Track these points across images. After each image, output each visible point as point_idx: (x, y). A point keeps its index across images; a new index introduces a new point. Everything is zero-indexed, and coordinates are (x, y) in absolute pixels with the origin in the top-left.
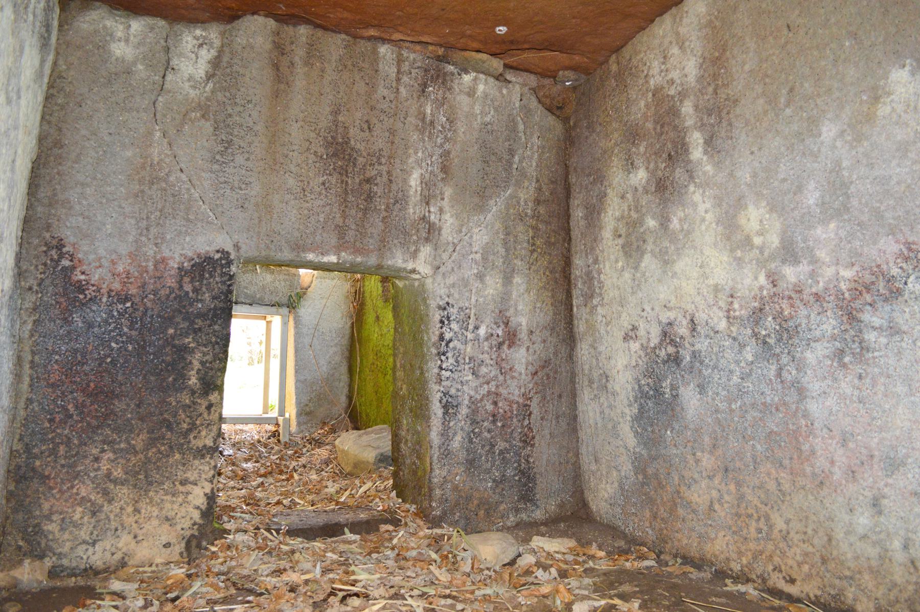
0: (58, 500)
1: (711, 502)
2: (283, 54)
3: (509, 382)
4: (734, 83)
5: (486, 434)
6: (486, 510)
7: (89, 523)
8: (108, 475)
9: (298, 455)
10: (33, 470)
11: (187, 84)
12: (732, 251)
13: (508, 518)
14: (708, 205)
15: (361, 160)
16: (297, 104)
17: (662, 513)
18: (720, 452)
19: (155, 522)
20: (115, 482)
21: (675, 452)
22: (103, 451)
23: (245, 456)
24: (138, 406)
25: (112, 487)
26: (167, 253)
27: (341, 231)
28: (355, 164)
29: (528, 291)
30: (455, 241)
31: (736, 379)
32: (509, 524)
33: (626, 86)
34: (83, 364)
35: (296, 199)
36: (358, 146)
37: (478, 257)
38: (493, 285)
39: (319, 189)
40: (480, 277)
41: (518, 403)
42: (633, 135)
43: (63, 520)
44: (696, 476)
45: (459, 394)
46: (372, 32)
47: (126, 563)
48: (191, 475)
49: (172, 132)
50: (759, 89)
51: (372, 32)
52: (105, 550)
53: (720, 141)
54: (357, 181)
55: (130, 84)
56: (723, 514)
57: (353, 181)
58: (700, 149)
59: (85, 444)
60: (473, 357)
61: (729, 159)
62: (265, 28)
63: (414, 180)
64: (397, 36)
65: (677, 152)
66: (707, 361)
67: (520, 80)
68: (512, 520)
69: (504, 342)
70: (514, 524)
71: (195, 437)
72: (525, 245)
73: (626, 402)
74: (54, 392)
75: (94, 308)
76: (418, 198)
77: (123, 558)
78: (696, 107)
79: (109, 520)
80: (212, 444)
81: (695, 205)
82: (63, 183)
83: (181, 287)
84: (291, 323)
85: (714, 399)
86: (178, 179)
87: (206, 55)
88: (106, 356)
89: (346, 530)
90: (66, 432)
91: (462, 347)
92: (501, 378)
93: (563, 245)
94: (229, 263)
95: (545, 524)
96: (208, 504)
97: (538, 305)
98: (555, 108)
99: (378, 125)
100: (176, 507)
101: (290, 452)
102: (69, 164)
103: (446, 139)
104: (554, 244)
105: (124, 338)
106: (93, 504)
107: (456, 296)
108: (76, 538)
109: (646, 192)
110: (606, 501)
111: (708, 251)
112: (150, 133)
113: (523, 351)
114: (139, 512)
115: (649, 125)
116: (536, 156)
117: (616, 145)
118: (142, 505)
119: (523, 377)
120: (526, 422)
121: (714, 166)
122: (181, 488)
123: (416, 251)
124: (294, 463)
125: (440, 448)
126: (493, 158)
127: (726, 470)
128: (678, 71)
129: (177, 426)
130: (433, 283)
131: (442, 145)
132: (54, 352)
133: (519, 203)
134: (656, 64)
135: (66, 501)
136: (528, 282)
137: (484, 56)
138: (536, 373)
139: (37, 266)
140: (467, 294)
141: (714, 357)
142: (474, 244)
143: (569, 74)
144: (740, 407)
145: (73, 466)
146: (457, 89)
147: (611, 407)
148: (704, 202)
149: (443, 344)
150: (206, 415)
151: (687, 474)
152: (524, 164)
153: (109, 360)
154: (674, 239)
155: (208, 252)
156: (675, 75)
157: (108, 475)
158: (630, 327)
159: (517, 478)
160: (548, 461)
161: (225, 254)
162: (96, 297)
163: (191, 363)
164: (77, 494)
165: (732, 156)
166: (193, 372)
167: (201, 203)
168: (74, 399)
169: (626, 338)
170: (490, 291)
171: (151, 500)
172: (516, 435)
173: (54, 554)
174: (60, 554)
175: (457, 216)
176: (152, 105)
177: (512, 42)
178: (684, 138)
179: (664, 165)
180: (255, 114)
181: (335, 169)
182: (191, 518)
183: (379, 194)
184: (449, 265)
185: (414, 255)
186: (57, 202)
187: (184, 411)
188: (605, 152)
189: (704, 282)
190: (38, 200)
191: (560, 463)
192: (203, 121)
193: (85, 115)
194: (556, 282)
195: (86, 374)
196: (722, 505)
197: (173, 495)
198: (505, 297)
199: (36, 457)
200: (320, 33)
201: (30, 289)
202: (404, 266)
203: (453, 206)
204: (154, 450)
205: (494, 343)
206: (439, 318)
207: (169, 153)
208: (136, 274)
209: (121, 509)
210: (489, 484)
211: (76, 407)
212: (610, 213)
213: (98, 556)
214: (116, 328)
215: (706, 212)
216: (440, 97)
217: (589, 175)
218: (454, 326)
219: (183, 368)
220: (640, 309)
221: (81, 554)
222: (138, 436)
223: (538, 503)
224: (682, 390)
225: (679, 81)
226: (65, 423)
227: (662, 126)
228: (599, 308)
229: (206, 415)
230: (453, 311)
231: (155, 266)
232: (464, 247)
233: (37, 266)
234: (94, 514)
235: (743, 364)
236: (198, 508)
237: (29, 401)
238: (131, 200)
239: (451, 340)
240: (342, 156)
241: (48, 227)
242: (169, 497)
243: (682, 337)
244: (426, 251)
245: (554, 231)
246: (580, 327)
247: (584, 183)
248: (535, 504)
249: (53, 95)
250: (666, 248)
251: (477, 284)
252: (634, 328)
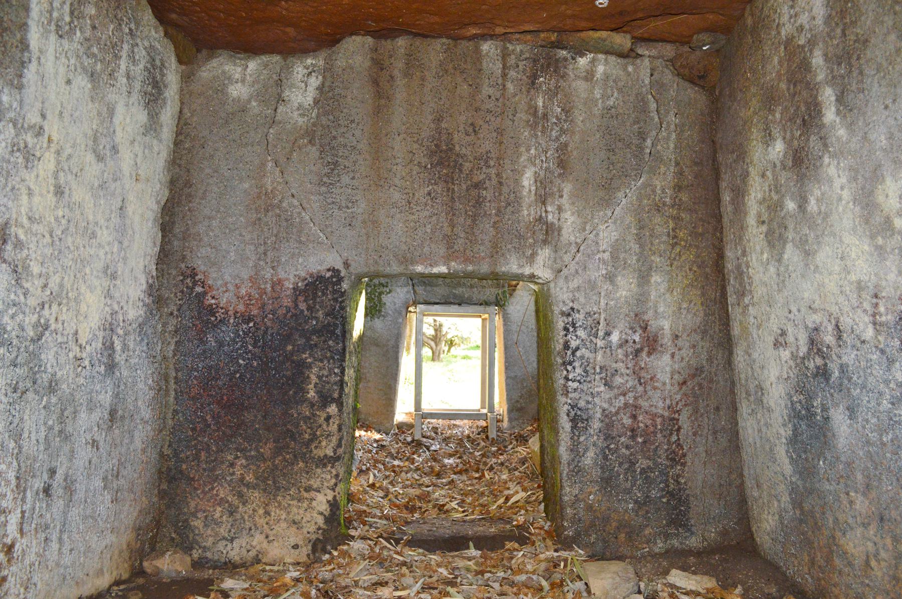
0: (201, 500)
1: (868, 556)
2: (382, 69)
3: (650, 393)
4: (863, 18)
5: (624, 450)
6: (627, 533)
7: (228, 522)
8: (242, 479)
9: (501, 451)
10: (181, 472)
11: (296, 113)
12: (872, 237)
13: (655, 543)
14: (844, 180)
15: (467, 166)
16: (398, 116)
17: (820, 560)
18: (873, 494)
19: (284, 525)
20: (248, 486)
21: (828, 487)
22: (237, 457)
23: (451, 451)
24: (264, 417)
25: (245, 490)
26: (282, 275)
27: (449, 241)
28: (461, 171)
29: (670, 290)
30: (578, 241)
31: (886, 404)
32: (657, 550)
33: (760, 42)
34: (217, 379)
35: (401, 212)
36: (464, 151)
37: (607, 256)
38: (626, 287)
39: (425, 200)
40: (610, 278)
41: (662, 416)
42: (770, 100)
43: (206, 517)
44: (850, 521)
45: (590, 406)
46: (474, 31)
47: (260, 560)
48: (315, 483)
49: (282, 160)
50: (889, 21)
51: (474, 31)
52: (241, 547)
53: (852, 96)
54: (464, 187)
55: (245, 121)
56: (879, 574)
57: (461, 188)
58: (833, 109)
59: (222, 451)
60: (605, 366)
61: (861, 118)
62: (363, 46)
63: (527, 180)
64: (499, 30)
65: (810, 115)
66: (855, 378)
67: (654, 52)
68: (660, 546)
69: (642, 349)
70: (663, 551)
71: (316, 447)
72: (665, 238)
73: (780, 420)
74: (195, 404)
75: (223, 329)
76: (533, 198)
77: (257, 555)
78: (825, 55)
79: (244, 521)
80: (332, 454)
81: (830, 181)
82: (193, 218)
83: (297, 305)
84: (498, 320)
85: (864, 427)
86: (291, 205)
87: (315, 81)
88: (236, 372)
89: (471, 544)
90: (206, 439)
91: (591, 356)
92: (640, 389)
93: (714, 235)
94: (340, 280)
95: (698, 554)
96: (331, 510)
97: (685, 305)
98: (696, 78)
99: (486, 126)
100: (301, 512)
101: (494, 449)
102: (197, 200)
103: (563, 131)
104: (702, 235)
105: (250, 356)
106: (230, 505)
107: (582, 300)
108: (217, 534)
109: (784, 167)
110: (768, 534)
111: (848, 239)
112: (263, 165)
113: (666, 358)
114: (270, 515)
115: (783, 86)
116: (674, 136)
117: (755, 113)
118: (272, 509)
119: (668, 387)
120: (674, 438)
121: (847, 128)
122: (306, 495)
123: (533, 255)
124: (494, 460)
125: (569, 464)
126: (620, 145)
127: (882, 519)
128: (807, 14)
129: (299, 436)
130: (555, 287)
131: (557, 138)
132: (193, 369)
133: (654, 191)
134: (785, 9)
135: (208, 501)
136: (670, 281)
137: (604, 34)
138: (684, 383)
139: (176, 294)
140: (594, 297)
141: (862, 373)
142: (601, 243)
143: (704, 37)
144: (892, 441)
145: (213, 470)
146: (572, 76)
147: (767, 425)
148: (839, 176)
149: (569, 353)
150: (325, 427)
151: (841, 517)
152: (659, 147)
153: (238, 375)
154: (813, 226)
155: (319, 272)
156: (804, 19)
157: (242, 479)
158: (779, 332)
159: (664, 500)
160: (704, 481)
161: (336, 272)
162: (224, 318)
163: (308, 377)
164: (217, 495)
165: (865, 113)
166: (312, 386)
167: (312, 225)
168: (211, 410)
169: (777, 344)
170: (623, 293)
171: (280, 503)
172: (661, 452)
173: (200, 547)
174: (205, 547)
175: (579, 214)
176: (264, 137)
177: (621, 13)
178: (816, 97)
179: (799, 132)
180: (358, 133)
181: (440, 178)
182: (316, 523)
183: (489, 199)
184: (573, 267)
185: (531, 259)
186: (189, 235)
187: (305, 423)
188: (745, 123)
189: (846, 278)
190: (174, 236)
191: (720, 485)
192: (310, 147)
193: (207, 155)
194: (707, 278)
195: (220, 389)
196: (878, 561)
197: (299, 501)
198: (642, 299)
199: (183, 461)
200: (418, 41)
201: (172, 314)
202: (520, 271)
203: (573, 203)
204: (280, 458)
205: (629, 350)
206: (563, 324)
207: (281, 181)
208: (257, 296)
209: (254, 510)
210: (631, 506)
211: (213, 418)
212: (753, 195)
213: (235, 552)
214: (242, 346)
215: (842, 188)
216: (552, 87)
217: (733, 152)
218: (581, 333)
219: (302, 382)
220: (786, 310)
221: (222, 548)
222: (266, 444)
223: (694, 529)
224: (832, 412)
225: (807, 27)
226: (205, 432)
227: (795, 85)
228: (750, 308)
229: (325, 427)
230: (579, 317)
231: (272, 287)
232: (588, 246)
233: (176, 294)
234: (231, 514)
235: (892, 385)
236: (321, 514)
237: (175, 412)
238: (250, 228)
239: (577, 349)
240: (447, 163)
241: (184, 258)
242: (295, 502)
243: (828, 347)
244: (544, 254)
245: (701, 219)
246: (736, 331)
247: (729, 162)
248: (689, 530)
249: (181, 141)
250: (806, 235)
251: (607, 286)
252: (783, 333)
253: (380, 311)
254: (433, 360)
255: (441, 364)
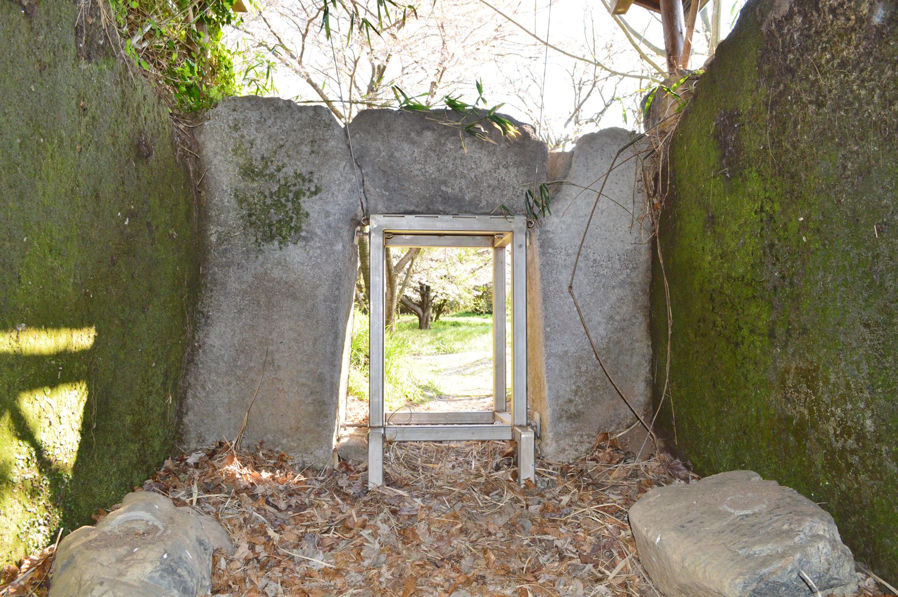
253: (298, 229)
254: (420, 327)
255: (429, 332)
